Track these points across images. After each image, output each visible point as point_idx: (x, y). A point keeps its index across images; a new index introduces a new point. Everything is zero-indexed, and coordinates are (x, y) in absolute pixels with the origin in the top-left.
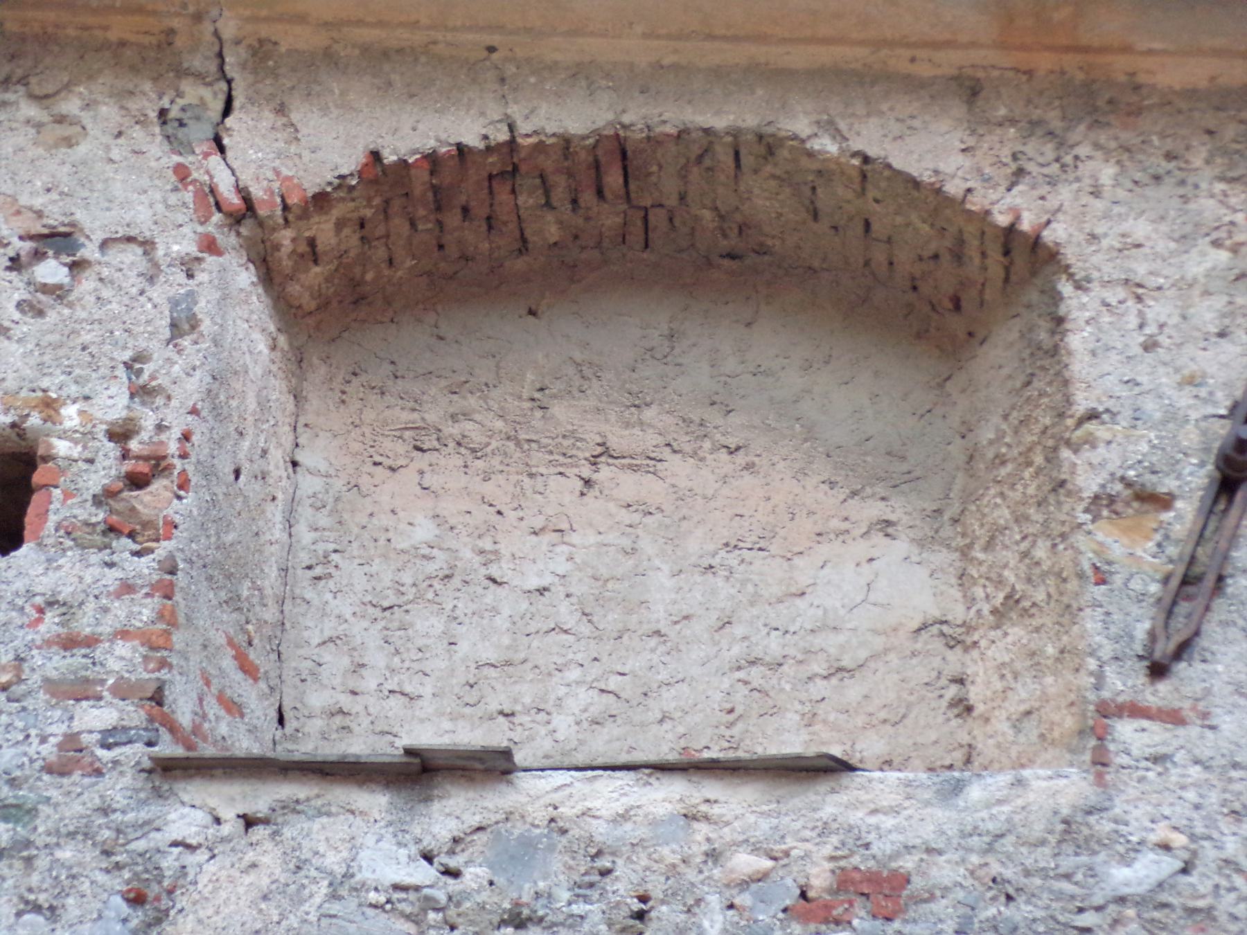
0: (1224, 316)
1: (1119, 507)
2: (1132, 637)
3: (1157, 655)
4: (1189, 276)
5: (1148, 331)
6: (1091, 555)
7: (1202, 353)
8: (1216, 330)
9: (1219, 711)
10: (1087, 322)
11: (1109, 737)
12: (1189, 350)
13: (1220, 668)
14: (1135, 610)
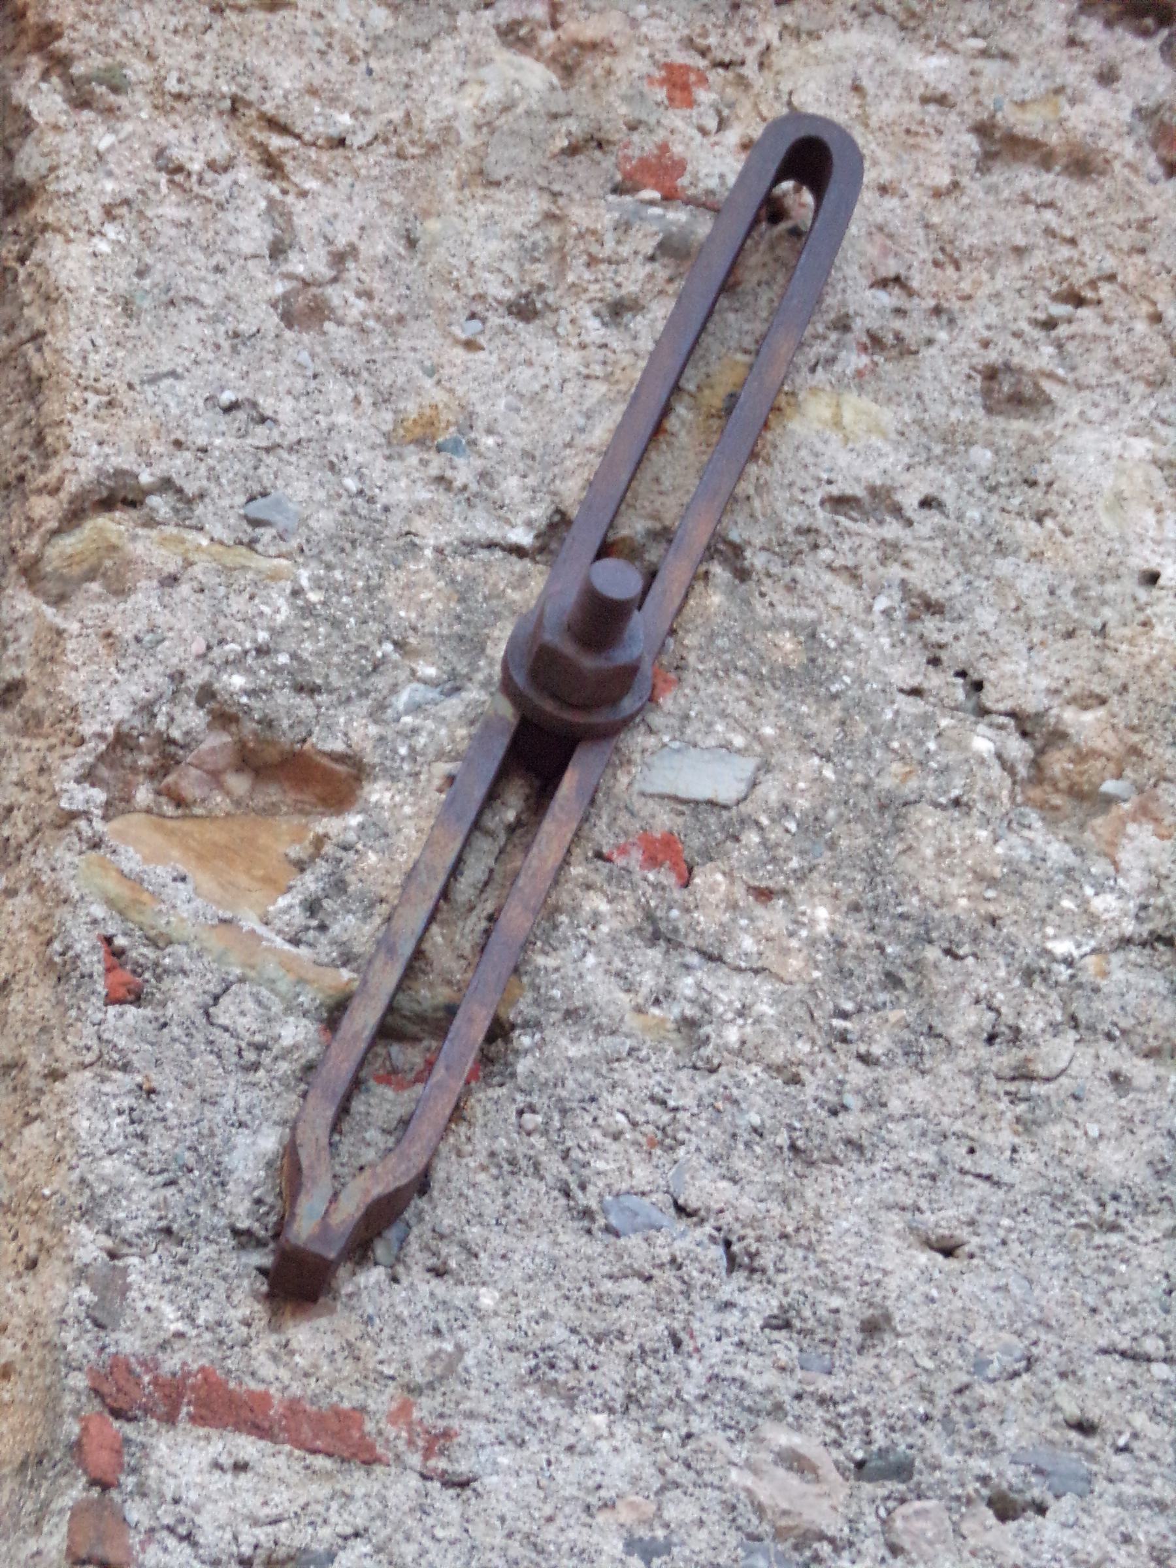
0: (530, 255)
1: (188, 781)
2: (220, 1176)
3: (303, 1229)
4: (430, 120)
5: (297, 264)
6: (98, 911)
7: (459, 354)
8: (508, 294)
9: (477, 1429)
10: (109, 213)
11: (130, 1482)
12: (425, 341)
13: (488, 1299)
14: (234, 1092)
